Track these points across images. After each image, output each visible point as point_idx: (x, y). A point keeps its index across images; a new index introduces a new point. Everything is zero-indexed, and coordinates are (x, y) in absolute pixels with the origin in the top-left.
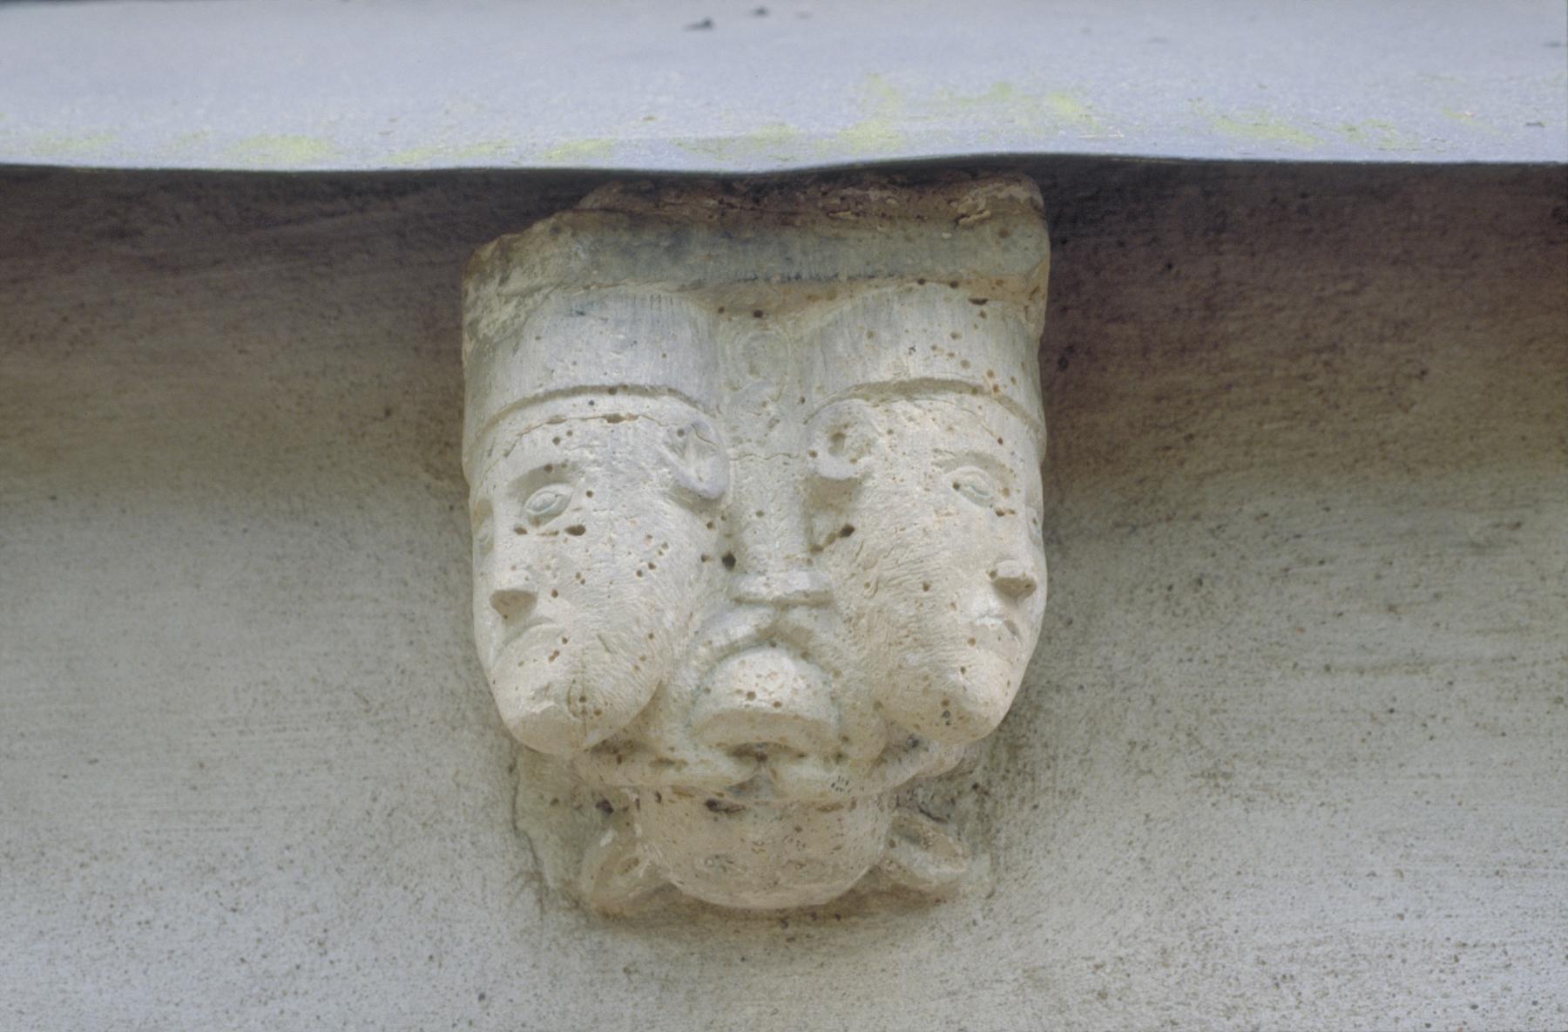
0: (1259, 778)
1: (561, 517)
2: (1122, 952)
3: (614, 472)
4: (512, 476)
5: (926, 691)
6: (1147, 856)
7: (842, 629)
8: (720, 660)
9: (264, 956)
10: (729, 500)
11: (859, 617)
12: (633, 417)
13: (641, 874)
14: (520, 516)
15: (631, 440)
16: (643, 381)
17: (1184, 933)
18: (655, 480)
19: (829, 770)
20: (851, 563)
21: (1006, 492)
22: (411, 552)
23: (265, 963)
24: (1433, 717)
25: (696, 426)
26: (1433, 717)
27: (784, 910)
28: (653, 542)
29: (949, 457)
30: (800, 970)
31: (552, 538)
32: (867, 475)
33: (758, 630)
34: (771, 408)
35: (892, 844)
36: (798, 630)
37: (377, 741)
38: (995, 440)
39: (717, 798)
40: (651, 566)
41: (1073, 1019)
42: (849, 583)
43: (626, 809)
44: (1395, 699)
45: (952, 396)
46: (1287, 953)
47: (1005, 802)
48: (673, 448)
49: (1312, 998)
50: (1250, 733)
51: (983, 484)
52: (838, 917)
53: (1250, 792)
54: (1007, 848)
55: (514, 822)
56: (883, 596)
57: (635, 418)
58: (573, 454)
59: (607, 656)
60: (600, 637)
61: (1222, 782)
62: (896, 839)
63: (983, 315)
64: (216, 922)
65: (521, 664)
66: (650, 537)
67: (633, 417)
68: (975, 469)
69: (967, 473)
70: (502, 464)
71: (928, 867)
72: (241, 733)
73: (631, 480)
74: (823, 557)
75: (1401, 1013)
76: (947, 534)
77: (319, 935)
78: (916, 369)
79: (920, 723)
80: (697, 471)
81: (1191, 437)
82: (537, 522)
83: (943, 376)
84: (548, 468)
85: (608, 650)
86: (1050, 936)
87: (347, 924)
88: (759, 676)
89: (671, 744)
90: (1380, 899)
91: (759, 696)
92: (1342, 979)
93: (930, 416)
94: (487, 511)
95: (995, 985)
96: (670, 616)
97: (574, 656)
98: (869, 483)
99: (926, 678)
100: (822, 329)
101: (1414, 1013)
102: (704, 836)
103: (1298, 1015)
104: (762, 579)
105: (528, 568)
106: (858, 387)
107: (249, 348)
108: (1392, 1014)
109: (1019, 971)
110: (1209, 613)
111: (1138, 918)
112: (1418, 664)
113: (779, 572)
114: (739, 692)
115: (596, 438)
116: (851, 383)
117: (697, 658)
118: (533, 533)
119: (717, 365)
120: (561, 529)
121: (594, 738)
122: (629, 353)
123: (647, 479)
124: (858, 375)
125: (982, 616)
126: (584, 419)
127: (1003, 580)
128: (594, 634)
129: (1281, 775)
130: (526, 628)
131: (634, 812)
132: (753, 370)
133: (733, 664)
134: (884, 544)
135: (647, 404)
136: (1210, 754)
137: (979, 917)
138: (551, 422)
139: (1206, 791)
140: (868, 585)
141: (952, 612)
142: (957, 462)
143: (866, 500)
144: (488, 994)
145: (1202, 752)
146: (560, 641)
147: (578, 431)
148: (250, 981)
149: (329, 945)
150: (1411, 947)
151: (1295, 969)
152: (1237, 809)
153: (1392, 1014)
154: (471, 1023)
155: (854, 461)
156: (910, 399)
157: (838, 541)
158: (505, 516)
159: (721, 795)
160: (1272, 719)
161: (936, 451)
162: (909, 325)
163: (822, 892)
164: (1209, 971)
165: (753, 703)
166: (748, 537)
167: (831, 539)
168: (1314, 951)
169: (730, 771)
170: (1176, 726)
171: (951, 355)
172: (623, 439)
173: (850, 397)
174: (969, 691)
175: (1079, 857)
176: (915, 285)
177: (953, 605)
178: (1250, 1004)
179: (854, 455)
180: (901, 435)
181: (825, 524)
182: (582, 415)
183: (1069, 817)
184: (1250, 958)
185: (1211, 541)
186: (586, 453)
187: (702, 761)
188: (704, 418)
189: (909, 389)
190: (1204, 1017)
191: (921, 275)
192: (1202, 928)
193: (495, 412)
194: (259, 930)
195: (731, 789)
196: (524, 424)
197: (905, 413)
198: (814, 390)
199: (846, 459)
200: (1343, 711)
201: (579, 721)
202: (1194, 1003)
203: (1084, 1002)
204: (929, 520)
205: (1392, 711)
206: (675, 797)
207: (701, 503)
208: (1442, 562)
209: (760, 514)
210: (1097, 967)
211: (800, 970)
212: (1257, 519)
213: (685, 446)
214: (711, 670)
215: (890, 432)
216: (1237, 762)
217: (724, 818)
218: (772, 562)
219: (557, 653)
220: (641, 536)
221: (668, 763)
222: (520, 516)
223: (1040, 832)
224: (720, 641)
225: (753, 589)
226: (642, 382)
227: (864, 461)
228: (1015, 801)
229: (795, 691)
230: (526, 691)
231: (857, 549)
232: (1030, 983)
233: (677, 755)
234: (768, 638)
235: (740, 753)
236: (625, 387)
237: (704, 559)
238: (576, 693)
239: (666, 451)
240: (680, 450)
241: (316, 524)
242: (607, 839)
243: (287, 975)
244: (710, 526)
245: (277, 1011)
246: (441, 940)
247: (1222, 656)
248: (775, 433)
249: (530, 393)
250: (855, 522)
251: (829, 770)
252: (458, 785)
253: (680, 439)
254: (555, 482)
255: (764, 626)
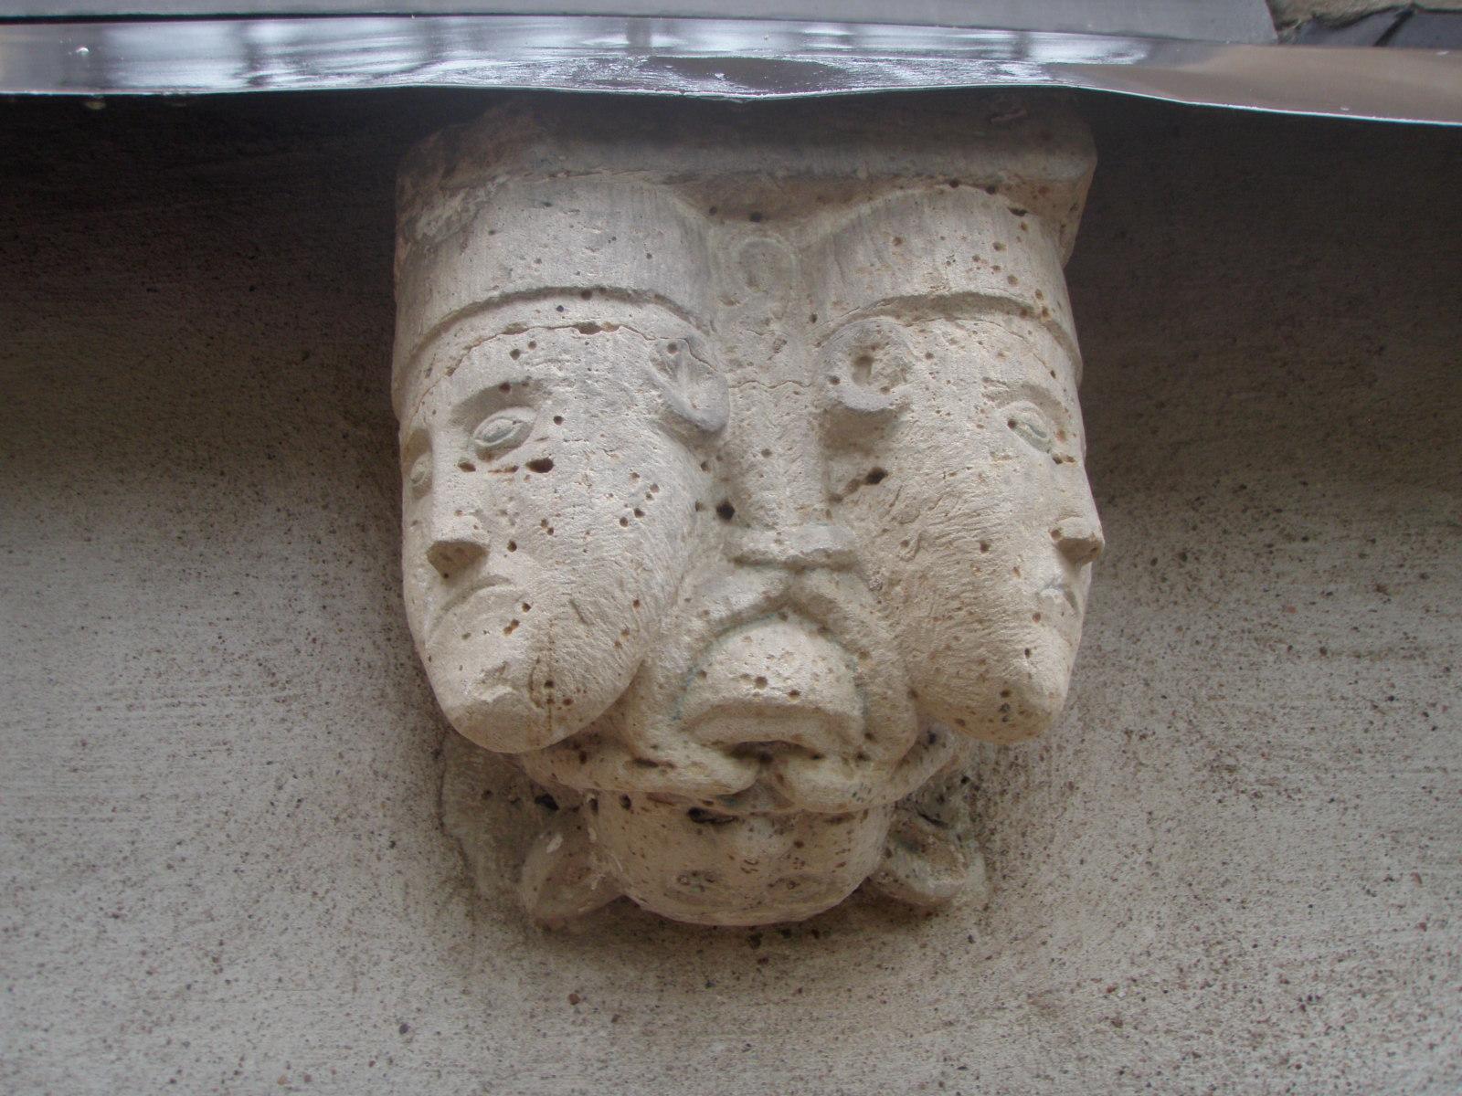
0: (1263, 771)
1: (521, 449)
2: (1135, 972)
3: (590, 394)
4: (456, 399)
5: (982, 678)
6: (1154, 860)
7: (868, 599)
8: (718, 635)
9: (149, 973)
10: (727, 435)
11: (892, 583)
12: (612, 328)
13: (594, 886)
14: (466, 448)
15: (611, 357)
16: (626, 283)
17: (1199, 949)
18: (642, 405)
19: (850, 776)
20: (881, 517)
21: (1062, 435)
22: (325, 507)
23: (150, 981)
24: (1434, 705)
25: (689, 341)
26: (1434, 705)
27: (753, 928)
28: (640, 482)
29: (1003, 388)
30: (775, 998)
31: (509, 475)
32: (904, 407)
33: (768, 599)
34: (775, 326)
35: (888, 854)
36: (818, 598)
37: (283, 720)
38: (1048, 372)
39: (704, 807)
40: (638, 513)
41: (1084, 1052)
42: (879, 541)
43: (576, 809)
44: (1393, 686)
45: (999, 317)
46: (1311, 970)
47: (997, 798)
48: (662, 366)
49: (1341, 1022)
50: (1251, 722)
51: (1040, 423)
52: (816, 933)
53: (1257, 787)
54: (1003, 853)
55: (440, 816)
56: (925, 559)
57: (615, 328)
58: (537, 371)
59: (581, 629)
60: (572, 603)
61: (1226, 775)
62: (892, 848)
63: (1023, 227)
64: (94, 931)
65: (466, 636)
66: (635, 476)
67: (612, 328)
68: (1032, 405)
69: (1022, 409)
70: (445, 384)
71: (928, 879)
72: (130, 707)
73: (611, 404)
74: (840, 511)
75: (1436, 1037)
76: (1007, 482)
77: (214, 948)
78: (957, 280)
79: (966, 718)
80: (691, 398)
81: (1162, 405)
82: (487, 455)
83: (990, 292)
84: (505, 387)
85: (582, 620)
86: (1055, 955)
87: (246, 934)
88: (771, 657)
89: (654, 741)
90: (1401, 907)
91: (772, 682)
92: (1372, 998)
93: (975, 338)
94: (423, 443)
95: (997, 1014)
96: (660, 576)
97: (538, 627)
98: (907, 417)
99: (983, 662)
100: (836, 236)
101: (1449, 1038)
102: (689, 851)
103: (1327, 1043)
104: (772, 534)
105: (478, 513)
106: (887, 301)
107: (159, 286)
108: (1426, 1039)
109: (1024, 996)
110: (1195, 591)
111: (1150, 933)
112: (1417, 652)
113: (792, 523)
114: (746, 676)
115: (566, 351)
116: (878, 296)
117: (689, 632)
118: (484, 470)
119: (709, 274)
120: (522, 464)
121: (560, 734)
122: (607, 251)
123: (631, 403)
124: (887, 288)
125: (1047, 586)
126: (550, 328)
127: (1069, 540)
128: (565, 599)
129: (1287, 769)
130: (474, 589)
131: (587, 813)
132: (752, 282)
133: (735, 642)
134: (930, 492)
135: (628, 313)
136: (1211, 745)
137: (974, 932)
138: (509, 332)
139: (1210, 786)
140: (905, 544)
141: (1015, 579)
142: (1011, 397)
143: (905, 437)
144: (411, 1023)
145: (1203, 742)
146: (519, 607)
147: (546, 343)
148: (132, 1003)
149: (224, 960)
150: (1438, 961)
151: (1320, 988)
152: (1243, 806)
153: (1426, 1039)
154: (391, 1061)
155: (885, 390)
156: (950, 318)
157: (863, 488)
158: (448, 447)
159: (709, 803)
160: (1271, 706)
161: (986, 380)
162: (945, 232)
163: (804, 910)
164: (1229, 993)
165: (764, 691)
166: (751, 482)
167: (854, 486)
168: (1339, 967)
169: (732, 775)
170: (1174, 713)
171: (996, 268)
172: (600, 353)
173: (877, 314)
174: (1035, 680)
175: (1082, 862)
176: (947, 187)
177: (1016, 570)
178: (1276, 1031)
179: (886, 383)
180: (943, 359)
181: (847, 468)
182: (548, 323)
183: (1067, 815)
184: (1272, 978)
185: (1192, 513)
186: (554, 369)
187: (695, 764)
188: (697, 333)
189: (950, 306)
190: (1230, 1047)
191: (955, 176)
192: (1219, 943)
193: (436, 322)
194: (144, 940)
195: (721, 797)
196: (474, 335)
197: (945, 334)
198: (829, 306)
199: (876, 386)
200: (1343, 698)
201: (542, 712)
202: (1216, 1031)
203: (1097, 1032)
204: (984, 464)
205: (1391, 699)
206: (650, 805)
207: (699, 438)
208: (1424, 541)
209: (766, 453)
210: (1110, 990)
211: (775, 998)
212: (1235, 492)
213: (677, 364)
214: (707, 648)
215: (929, 356)
216: (1239, 753)
217: (710, 831)
218: (782, 513)
219: (516, 623)
220: (625, 473)
221: (651, 764)
222: (466, 448)
223: (1038, 834)
224: (719, 612)
225: (761, 547)
226: (623, 285)
227: (899, 390)
228: (1008, 796)
229: (816, 676)
230: (473, 672)
231: (891, 497)
232: (1036, 1010)
233: (661, 755)
234: (777, 608)
235: (740, 752)
236: (602, 290)
237: (698, 507)
238: (540, 676)
239: (653, 370)
240: (671, 369)
241: (222, 474)
242: (555, 843)
243: (176, 996)
244: (704, 466)
245: (163, 1041)
246: (355, 959)
247: (1214, 638)
248: (780, 357)
249: (482, 297)
250: (888, 464)
251: (850, 776)
252: (376, 773)
253: (672, 356)
254: (512, 405)
255: (774, 594)
